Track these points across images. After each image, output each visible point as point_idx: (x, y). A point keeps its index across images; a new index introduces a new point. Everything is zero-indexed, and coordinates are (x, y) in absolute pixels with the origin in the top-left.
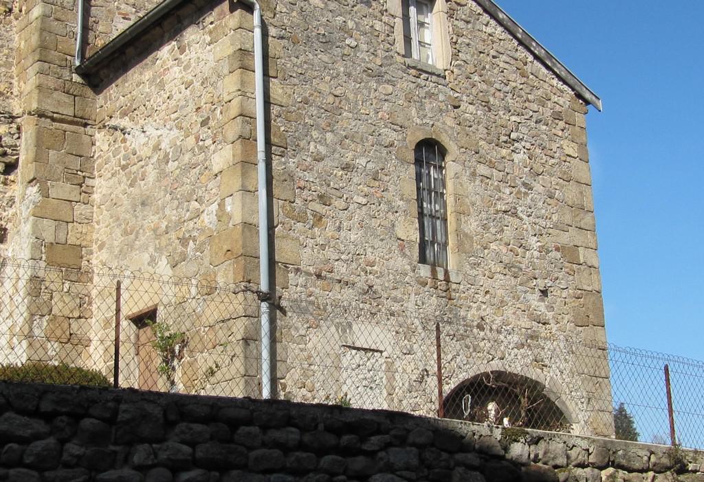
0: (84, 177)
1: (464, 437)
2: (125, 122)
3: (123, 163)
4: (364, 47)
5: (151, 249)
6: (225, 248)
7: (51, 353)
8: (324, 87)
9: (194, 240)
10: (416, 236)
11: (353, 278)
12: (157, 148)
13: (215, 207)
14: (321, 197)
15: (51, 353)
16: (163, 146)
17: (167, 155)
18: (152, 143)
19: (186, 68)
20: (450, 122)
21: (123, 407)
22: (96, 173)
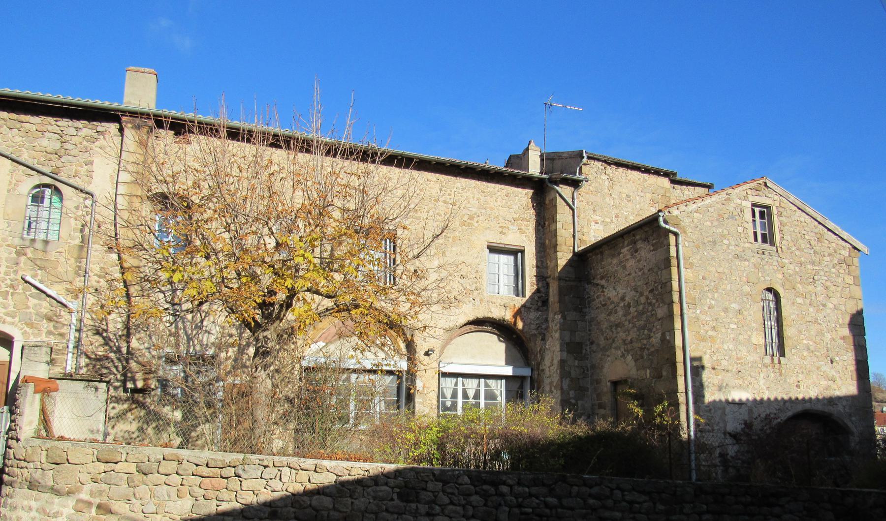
0: (582, 308)
1: (589, 283)
2: (603, 282)
3: (603, 303)
4: (733, 243)
5: (622, 350)
6: (666, 357)
7: (571, 396)
8: (713, 269)
9: (648, 349)
10: (762, 341)
11: (730, 368)
12: (623, 299)
13: (659, 335)
14: (714, 328)
15: (571, 396)
16: (627, 298)
17: (629, 304)
18: (620, 296)
19: (639, 261)
20: (780, 276)
21: (678, 489)
22: (587, 306)
